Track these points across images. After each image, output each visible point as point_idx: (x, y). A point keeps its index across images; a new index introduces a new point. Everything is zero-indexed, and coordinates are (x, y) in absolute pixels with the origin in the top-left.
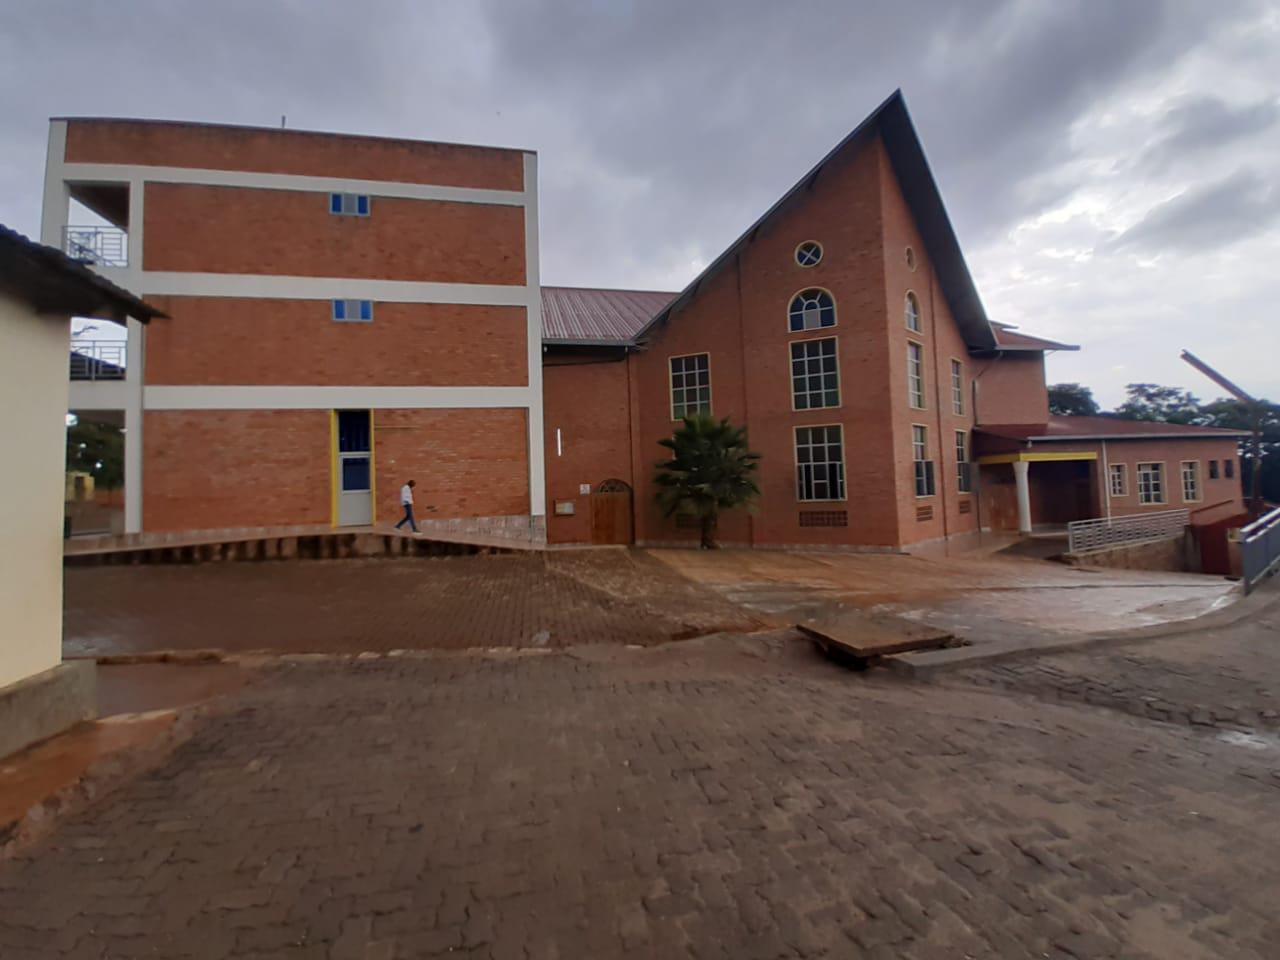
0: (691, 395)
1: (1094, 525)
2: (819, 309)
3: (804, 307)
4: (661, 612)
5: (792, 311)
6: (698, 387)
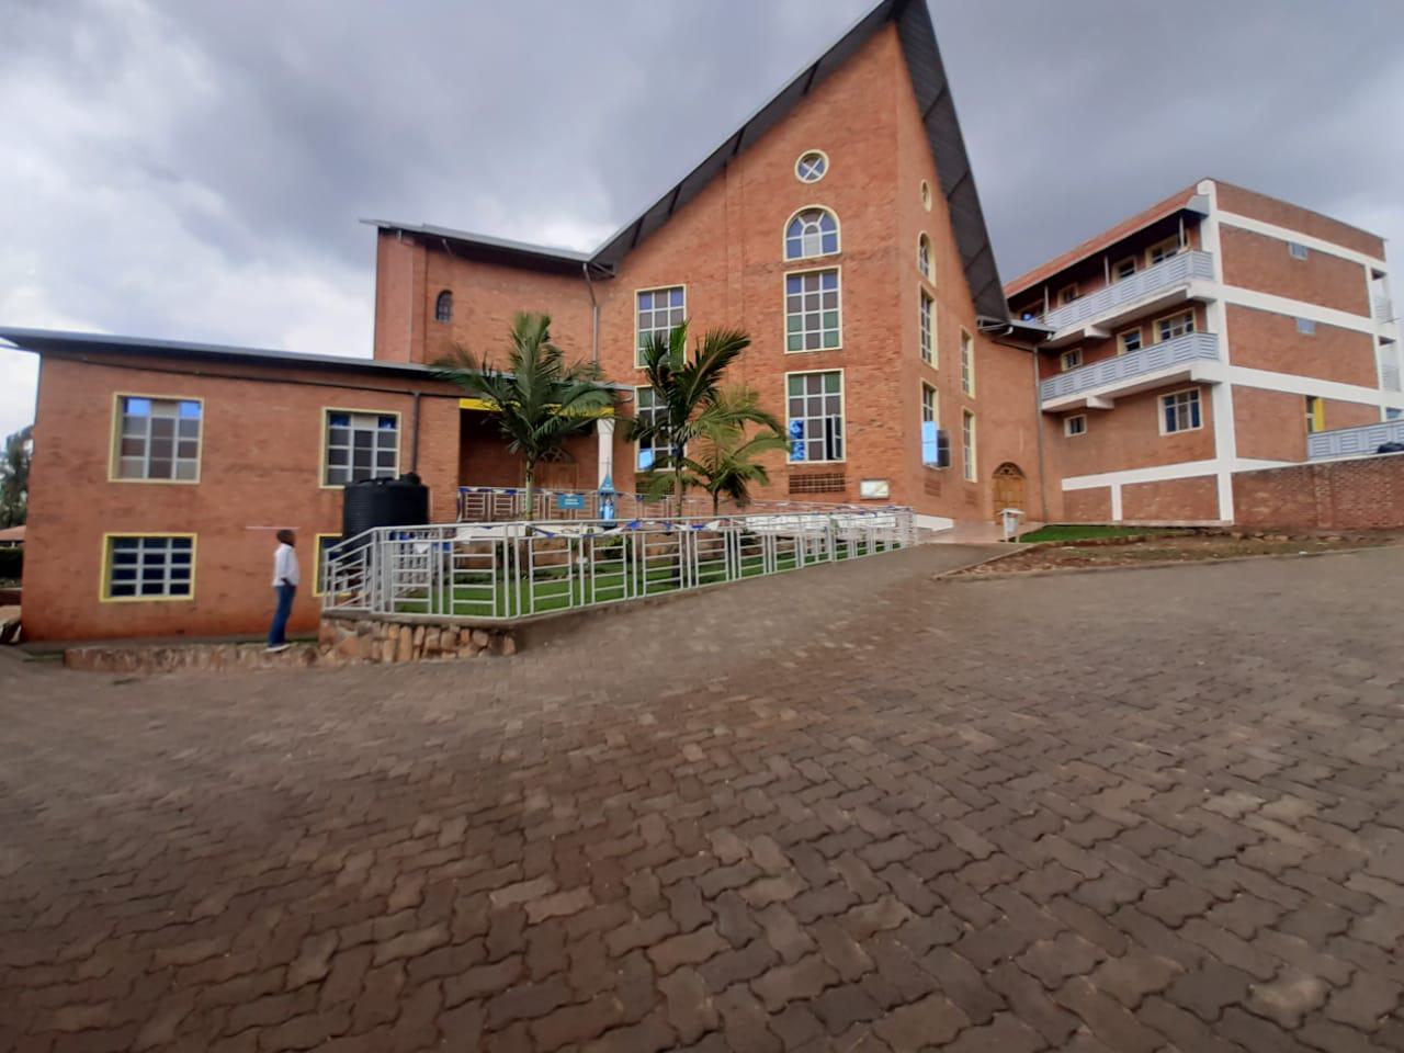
0: (813, 322)
1: (1171, 285)
2: (820, 234)
3: (803, 232)
4: (950, 729)
5: (788, 235)
6: (821, 311)
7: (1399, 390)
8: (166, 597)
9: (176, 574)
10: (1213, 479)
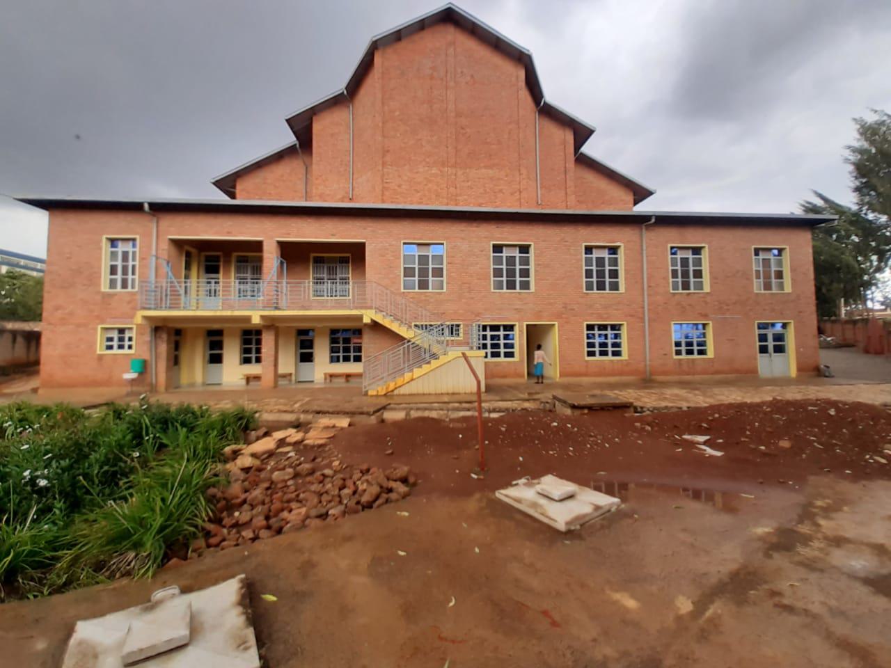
7: (287, 120)
8: (502, 359)
9: (506, 346)
10: (520, 257)
